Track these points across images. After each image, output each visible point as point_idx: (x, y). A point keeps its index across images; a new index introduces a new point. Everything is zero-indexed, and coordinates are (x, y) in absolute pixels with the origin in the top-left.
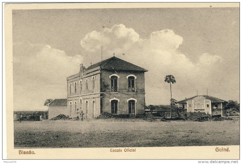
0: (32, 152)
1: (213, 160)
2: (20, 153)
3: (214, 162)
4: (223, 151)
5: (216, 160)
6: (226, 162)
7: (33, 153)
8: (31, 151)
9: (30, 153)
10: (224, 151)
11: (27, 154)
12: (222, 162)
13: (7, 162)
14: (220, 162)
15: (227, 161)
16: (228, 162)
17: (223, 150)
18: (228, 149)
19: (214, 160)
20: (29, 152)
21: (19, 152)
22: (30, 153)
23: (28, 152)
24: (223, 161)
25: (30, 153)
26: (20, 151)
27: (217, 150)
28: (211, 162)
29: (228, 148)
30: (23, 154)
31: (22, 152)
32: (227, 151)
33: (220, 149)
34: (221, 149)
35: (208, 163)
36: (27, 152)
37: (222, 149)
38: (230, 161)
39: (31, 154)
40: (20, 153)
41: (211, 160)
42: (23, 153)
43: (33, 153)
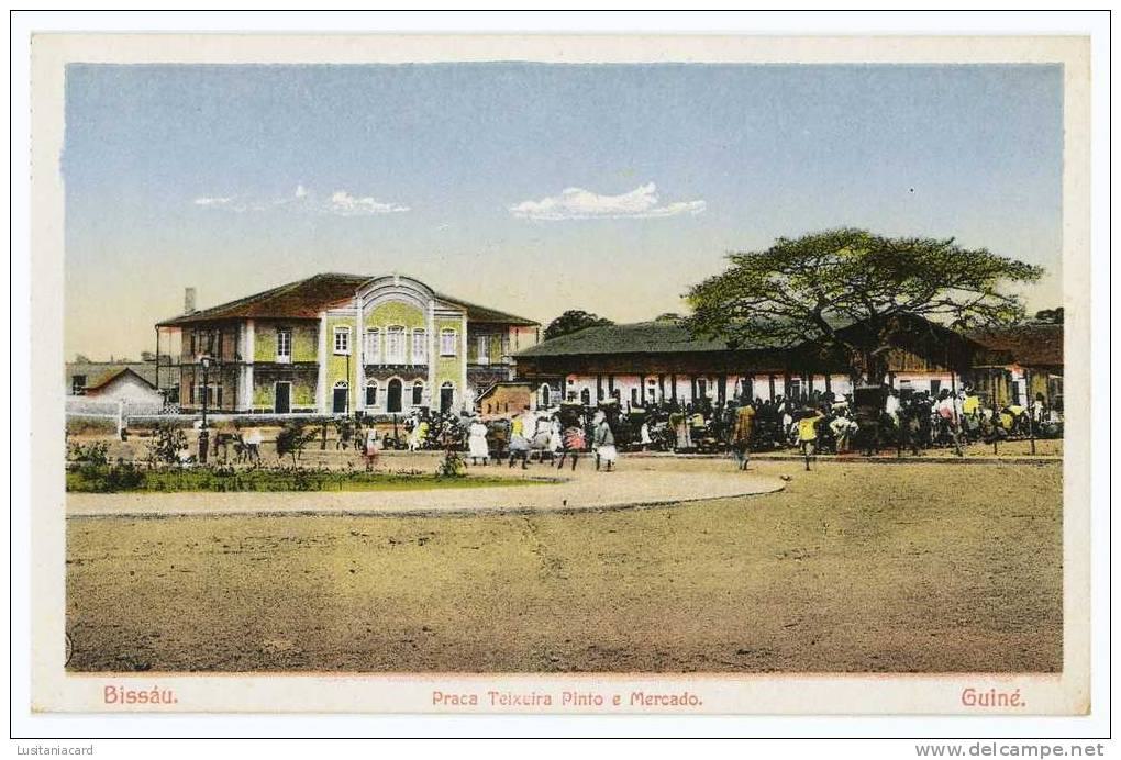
1: (983, 743)
2: (111, 698)
5: (1000, 744)
6: (1046, 751)
7: (167, 699)
12: (1027, 750)
18: (1018, 696)
19: (990, 743)
21: (107, 695)
24: (1030, 748)
26: (110, 690)
28: (974, 751)
31: (118, 692)
34: (987, 695)
35: (961, 754)
38: (1066, 745)
40: (111, 698)
41: (974, 742)
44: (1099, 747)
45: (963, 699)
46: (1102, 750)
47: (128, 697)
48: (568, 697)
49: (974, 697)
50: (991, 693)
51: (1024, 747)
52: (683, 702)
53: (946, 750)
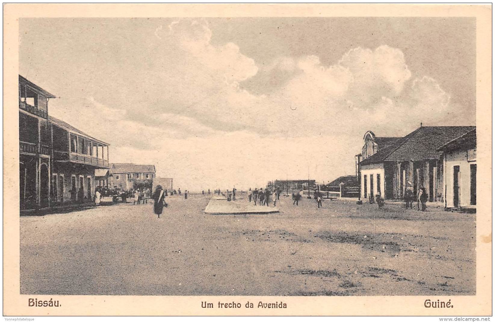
0: (444, 305)
1: (458, 317)
3: (459, 319)
4: (440, 306)
5: (463, 317)
6: (474, 319)
7: (56, 305)
8: (53, 300)
9: (51, 305)
10: (210, 307)
11: (44, 306)
12: (469, 319)
13: (22, 320)
14: (467, 319)
15: (476, 318)
16: (478, 319)
17: (55, 302)
18: (450, 303)
19: (460, 317)
20: (48, 301)
21: (30, 302)
22: (51, 304)
23: (46, 301)
24: (470, 319)
25: (51, 305)
26: (31, 300)
27: (428, 305)
28: (456, 319)
29: (450, 300)
30: (36, 306)
31: (35, 301)
32: (448, 307)
33: (434, 303)
34: (436, 302)
35: (452, 320)
36: (45, 302)
37: (277, 304)
38: (480, 318)
39: (52, 306)
40: (32, 304)
41: (456, 317)
42: (38, 304)
43: (56, 305)
44: (489, 318)
45: (425, 303)
46: (489, 319)
47: (39, 303)
48: (220, 305)
49: (52, 302)
50: (437, 302)
51: (469, 319)
52: (280, 306)
53: (448, 319)
